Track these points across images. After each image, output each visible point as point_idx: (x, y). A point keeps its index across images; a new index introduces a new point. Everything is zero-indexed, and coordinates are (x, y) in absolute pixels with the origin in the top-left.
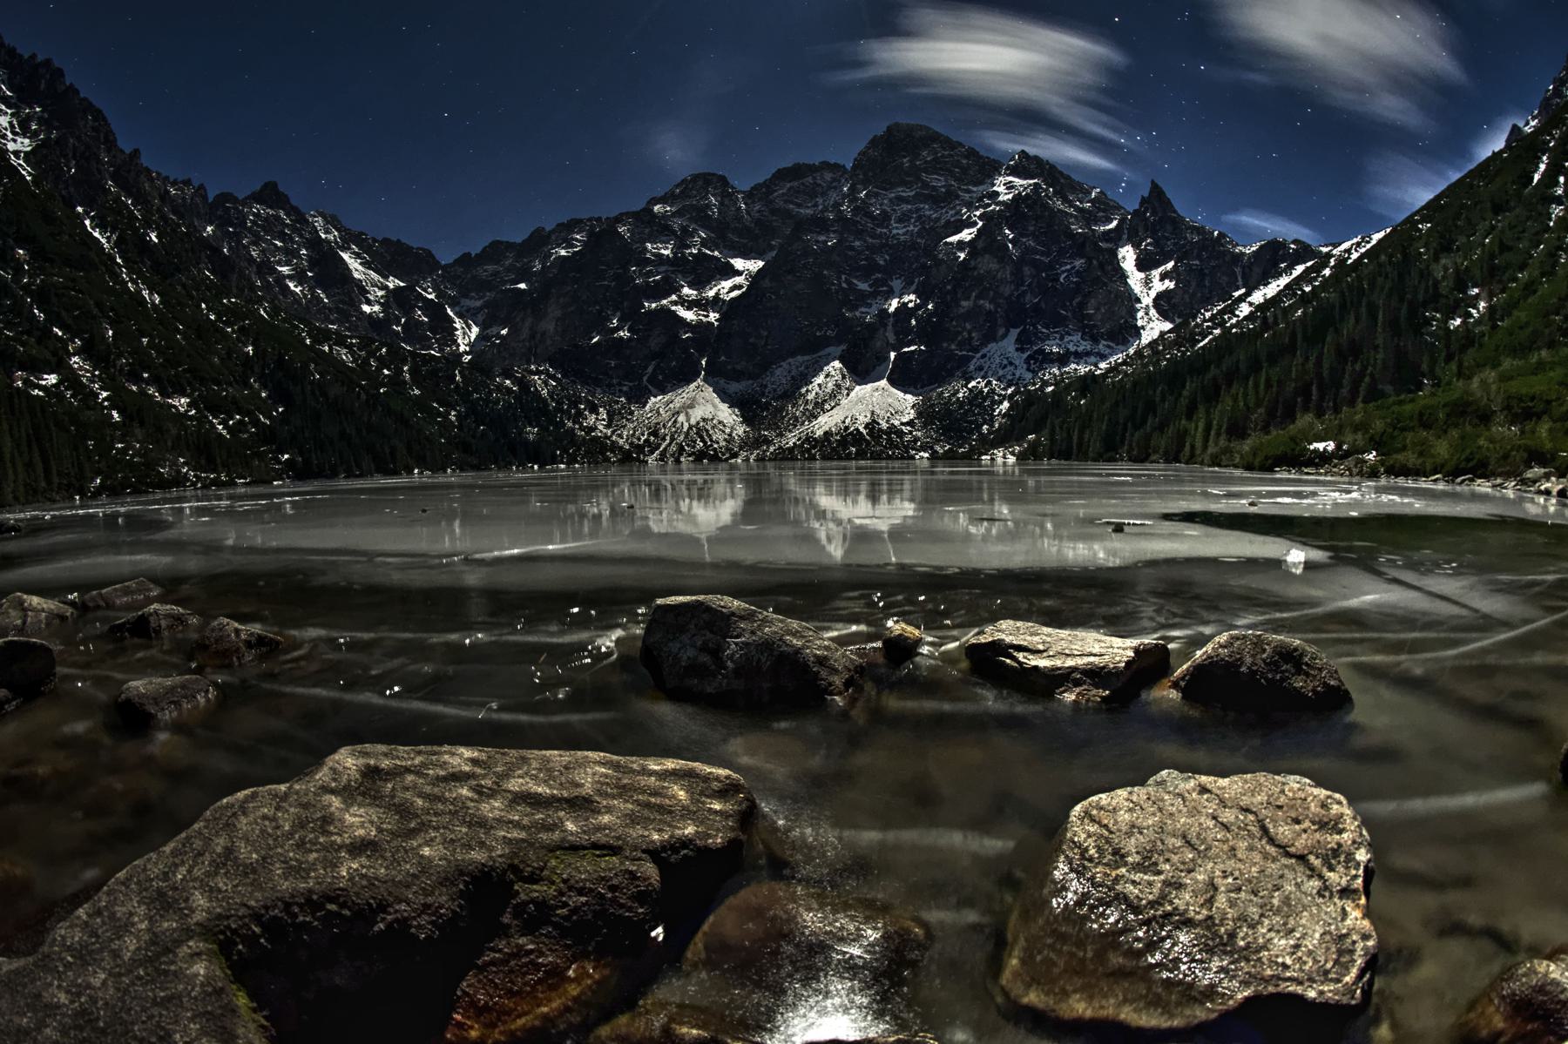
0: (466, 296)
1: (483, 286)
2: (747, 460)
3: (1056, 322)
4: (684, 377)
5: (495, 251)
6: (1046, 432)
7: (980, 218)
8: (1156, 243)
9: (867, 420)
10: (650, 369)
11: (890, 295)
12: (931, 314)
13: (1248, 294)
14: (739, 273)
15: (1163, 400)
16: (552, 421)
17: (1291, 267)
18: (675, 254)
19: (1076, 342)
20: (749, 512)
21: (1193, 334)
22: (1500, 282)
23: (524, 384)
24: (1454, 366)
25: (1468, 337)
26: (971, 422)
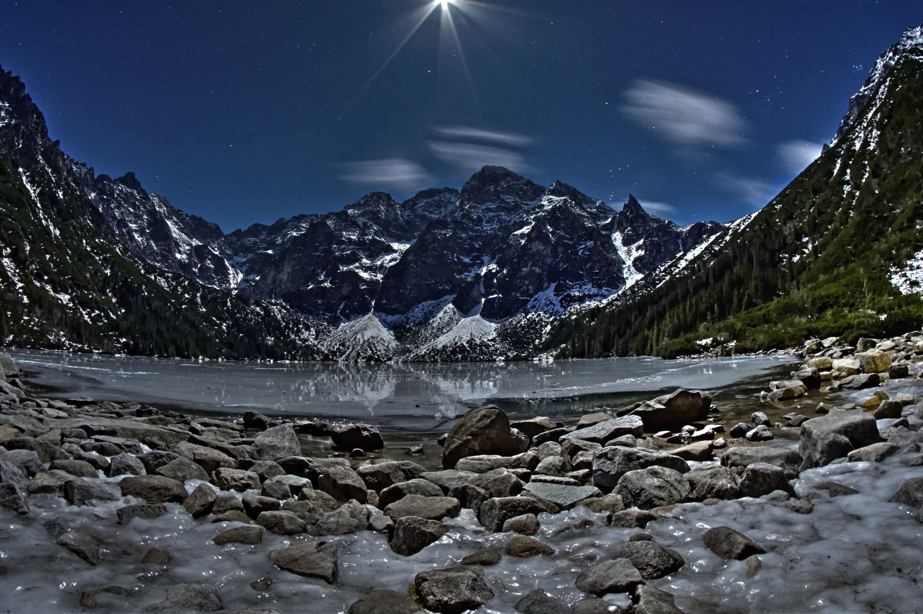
0: (236, 254)
1: (247, 250)
2: (397, 362)
3: (577, 278)
4: (364, 311)
5: (255, 230)
6: (570, 343)
7: (533, 220)
8: (633, 230)
9: (468, 339)
10: (342, 306)
11: (482, 264)
12: (505, 277)
13: (685, 255)
14: (395, 251)
15: (636, 319)
16: (283, 334)
17: (708, 237)
18: (359, 239)
19: (589, 289)
20: (400, 389)
21: (654, 280)
22: (819, 232)
23: (266, 310)
24: (795, 282)
25: (803, 265)
26: (529, 338)
